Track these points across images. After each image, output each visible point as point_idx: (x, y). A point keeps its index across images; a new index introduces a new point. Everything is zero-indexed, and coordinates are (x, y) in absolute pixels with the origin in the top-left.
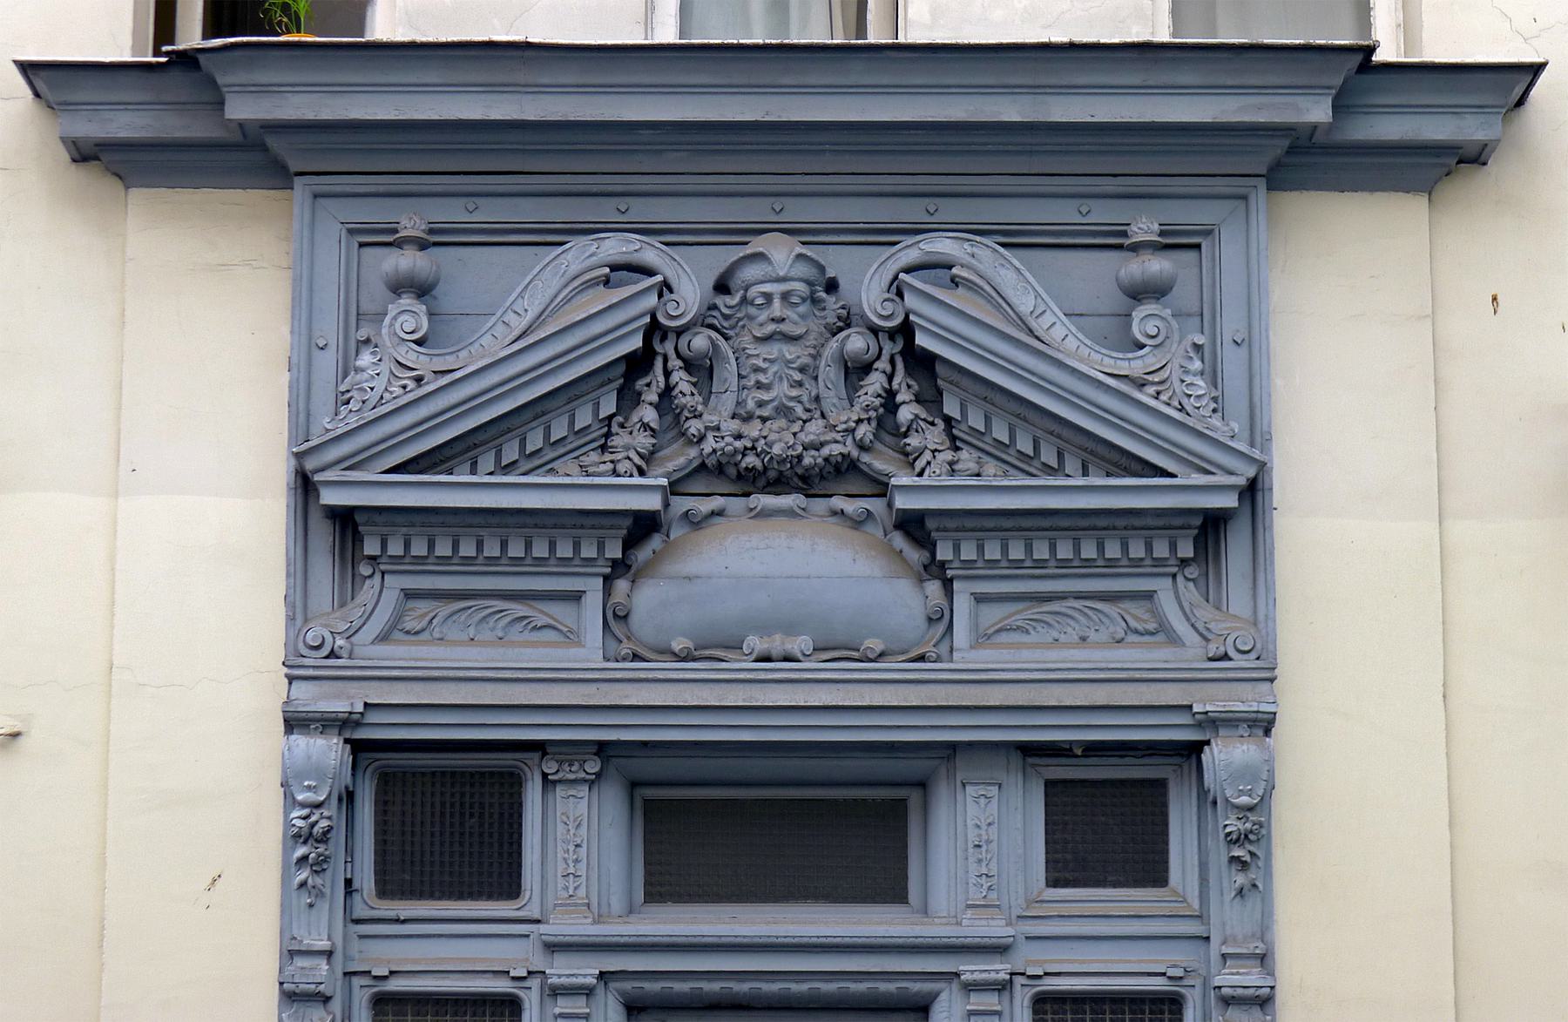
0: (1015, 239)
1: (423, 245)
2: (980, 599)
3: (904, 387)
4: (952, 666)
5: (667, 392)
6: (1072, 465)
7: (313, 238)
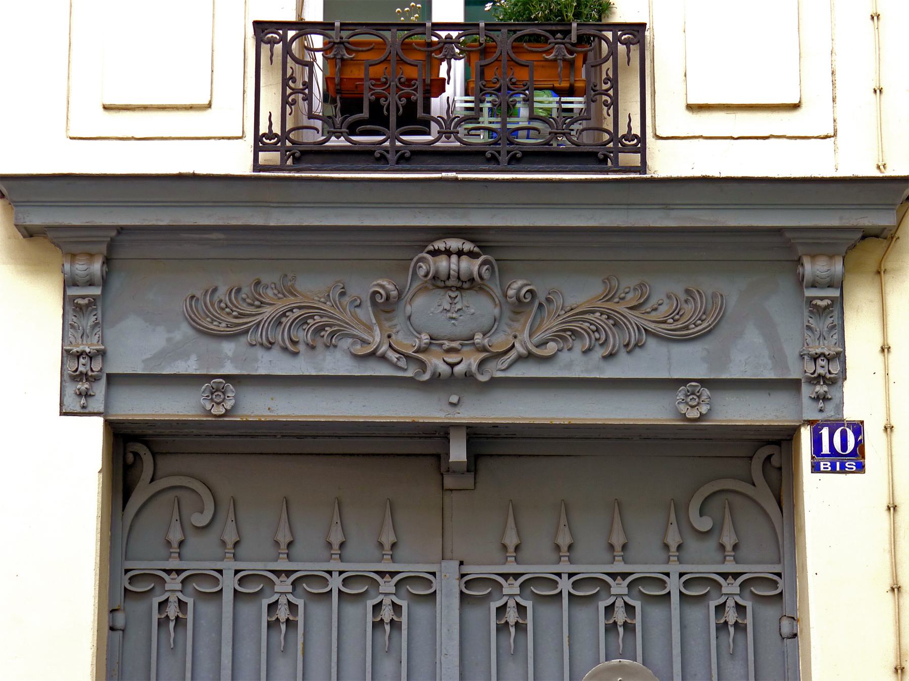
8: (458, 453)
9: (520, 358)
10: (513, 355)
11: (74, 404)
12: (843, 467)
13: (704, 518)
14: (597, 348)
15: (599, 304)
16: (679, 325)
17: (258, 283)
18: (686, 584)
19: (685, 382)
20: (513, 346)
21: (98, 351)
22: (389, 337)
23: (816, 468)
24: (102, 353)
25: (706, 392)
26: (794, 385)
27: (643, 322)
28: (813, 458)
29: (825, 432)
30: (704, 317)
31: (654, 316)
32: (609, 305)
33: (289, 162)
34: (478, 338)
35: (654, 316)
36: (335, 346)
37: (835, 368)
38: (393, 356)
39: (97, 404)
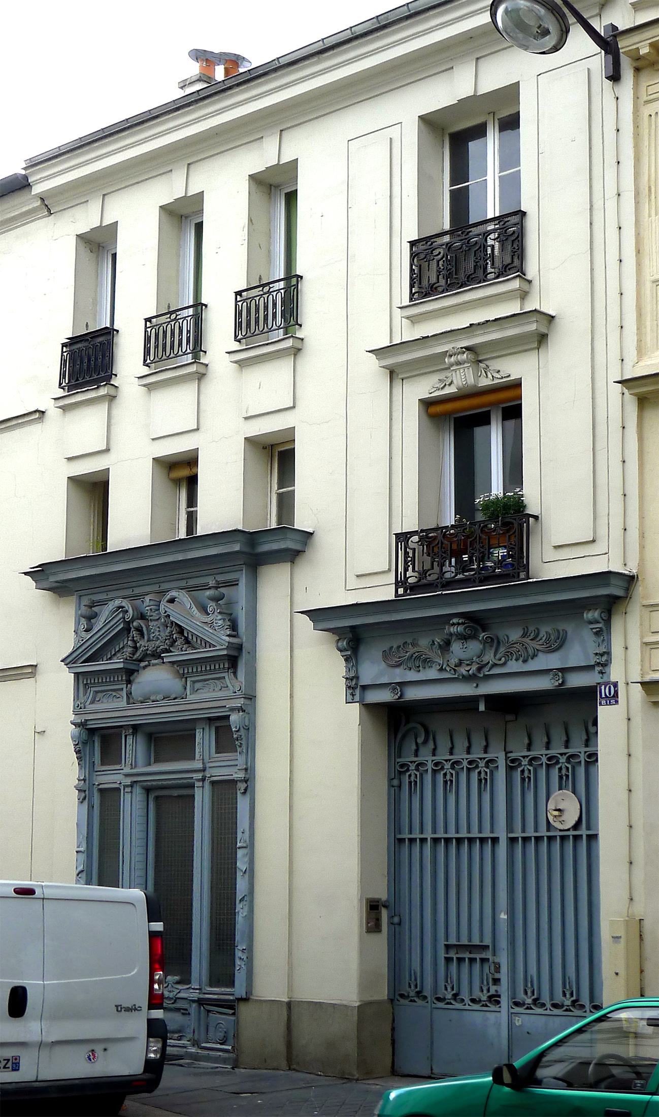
0: (189, 589)
2: (194, 682)
8: (482, 708)
10: (490, 665)
11: (350, 698)
12: (610, 702)
19: (551, 670)
20: (489, 662)
23: (601, 704)
29: (603, 687)
37: (604, 659)
39: (357, 698)
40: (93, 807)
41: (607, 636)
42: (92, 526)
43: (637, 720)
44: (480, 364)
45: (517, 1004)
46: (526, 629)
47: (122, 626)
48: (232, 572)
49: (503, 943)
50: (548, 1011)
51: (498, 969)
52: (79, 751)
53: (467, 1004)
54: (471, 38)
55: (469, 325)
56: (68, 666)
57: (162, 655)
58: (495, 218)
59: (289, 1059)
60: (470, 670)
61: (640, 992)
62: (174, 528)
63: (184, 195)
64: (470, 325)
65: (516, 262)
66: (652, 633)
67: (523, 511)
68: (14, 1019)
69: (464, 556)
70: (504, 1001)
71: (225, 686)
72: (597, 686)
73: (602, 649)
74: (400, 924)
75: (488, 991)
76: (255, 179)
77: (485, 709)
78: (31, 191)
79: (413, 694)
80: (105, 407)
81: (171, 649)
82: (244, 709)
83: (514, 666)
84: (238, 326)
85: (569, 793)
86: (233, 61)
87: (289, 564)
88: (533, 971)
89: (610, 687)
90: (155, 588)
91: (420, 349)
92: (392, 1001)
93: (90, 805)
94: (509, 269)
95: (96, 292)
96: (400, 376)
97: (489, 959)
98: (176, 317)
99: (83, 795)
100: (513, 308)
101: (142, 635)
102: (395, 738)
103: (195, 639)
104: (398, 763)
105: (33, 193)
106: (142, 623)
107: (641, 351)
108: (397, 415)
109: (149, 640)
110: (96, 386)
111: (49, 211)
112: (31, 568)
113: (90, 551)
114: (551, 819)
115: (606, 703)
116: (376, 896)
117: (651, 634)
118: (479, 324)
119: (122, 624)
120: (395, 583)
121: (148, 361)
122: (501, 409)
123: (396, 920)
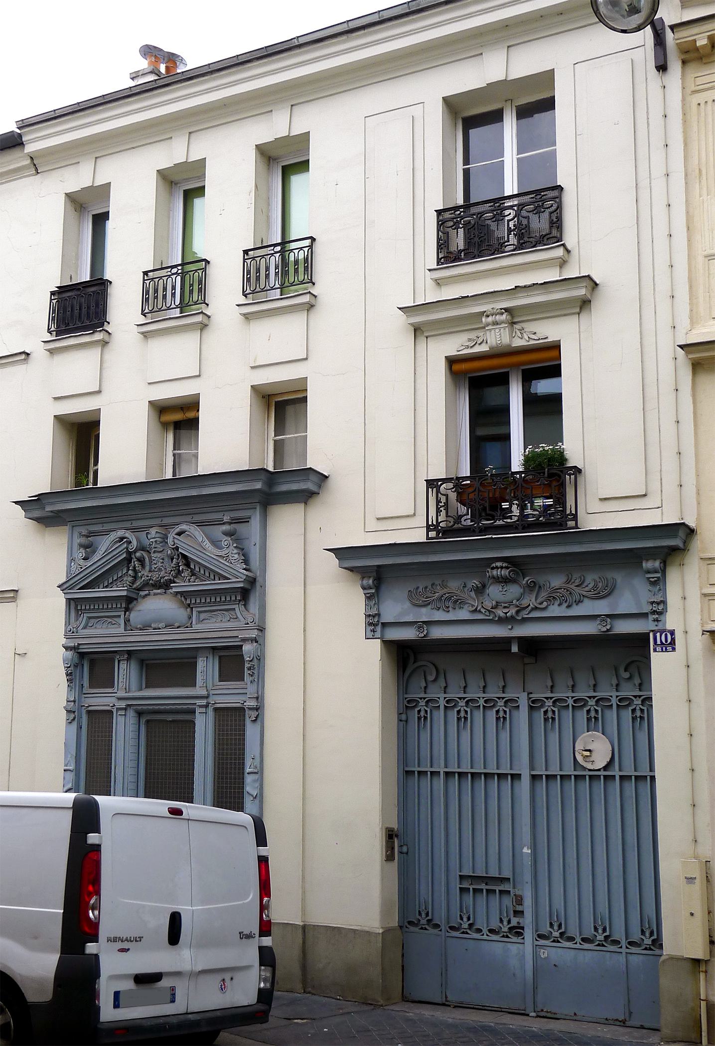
0: (200, 524)
1: (230, 523)
2: (200, 612)
3: (181, 562)
4: (192, 629)
5: (135, 567)
6: (217, 578)
7: (72, 537)
8: (515, 649)
9: (533, 609)
10: (530, 608)
11: (370, 635)
12: (666, 649)
13: (627, 672)
14: (564, 603)
15: (564, 585)
16: (596, 592)
17: (433, 584)
18: (620, 700)
20: (529, 605)
21: (376, 614)
22: (482, 603)
23: (655, 650)
24: (379, 615)
25: (609, 620)
26: (644, 615)
27: (581, 592)
28: (654, 646)
29: (658, 635)
30: (606, 588)
31: (587, 589)
32: (567, 585)
33: (441, 535)
34: (514, 602)
35: (587, 589)
36: (463, 608)
37: (661, 607)
38: (483, 610)
39: (378, 634)
40: (81, 728)
41: (663, 586)
42: (70, 463)
43: (698, 667)
44: (515, 326)
45: (541, 936)
46: (582, 577)
47: (124, 555)
48: (239, 510)
49: (527, 876)
50: (578, 945)
51: (519, 900)
52: (71, 673)
53: (485, 934)
54: (507, 26)
55: (513, 287)
56: (64, 592)
57: (171, 585)
58: (513, 195)
59: (304, 982)
60: (508, 612)
61: (708, 933)
62: (162, 467)
63: (287, 134)
64: (516, 286)
65: (555, 232)
66: (710, 585)
67: (563, 464)
68: (174, 946)
69: (503, 504)
70: (528, 934)
71: (235, 617)
72: (649, 633)
73: (658, 598)
74: (407, 853)
75: (509, 922)
76: (71, 198)
77: (518, 650)
78: (24, 149)
79: (438, 633)
80: (96, 352)
81: (175, 579)
82: (258, 640)
83: (555, 610)
84: (145, 300)
85: (600, 734)
86: (172, 59)
87: (303, 505)
88: (603, 907)
89: (666, 635)
90: (157, 521)
91: (455, 308)
92: (401, 927)
93: (79, 726)
94: (548, 239)
95: (78, 248)
96: (426, 334)
97: (510, 891)
98: (171, 270)
99: (72, 716)
100: (553, 275)
101: (143, 565)
102: (404, 672)
103: (202, 572)
104: (406, 698)
105: (25, 152)
106: (145, 555)
107: (694, 319)
108: (421, 370)
109: (150, 571)
110: (92, 331)
111: (36, 169)
112: (29, 497)
113: (68, 486)
114: (579, 758)
115: (662, 649)
116: (391, 826)
117: (708, 586)
118: (525, 287)
119: (125, 554)
120: (426, 527)
121: (147, 311)
122: (521, 371)
123: (405, 849)
